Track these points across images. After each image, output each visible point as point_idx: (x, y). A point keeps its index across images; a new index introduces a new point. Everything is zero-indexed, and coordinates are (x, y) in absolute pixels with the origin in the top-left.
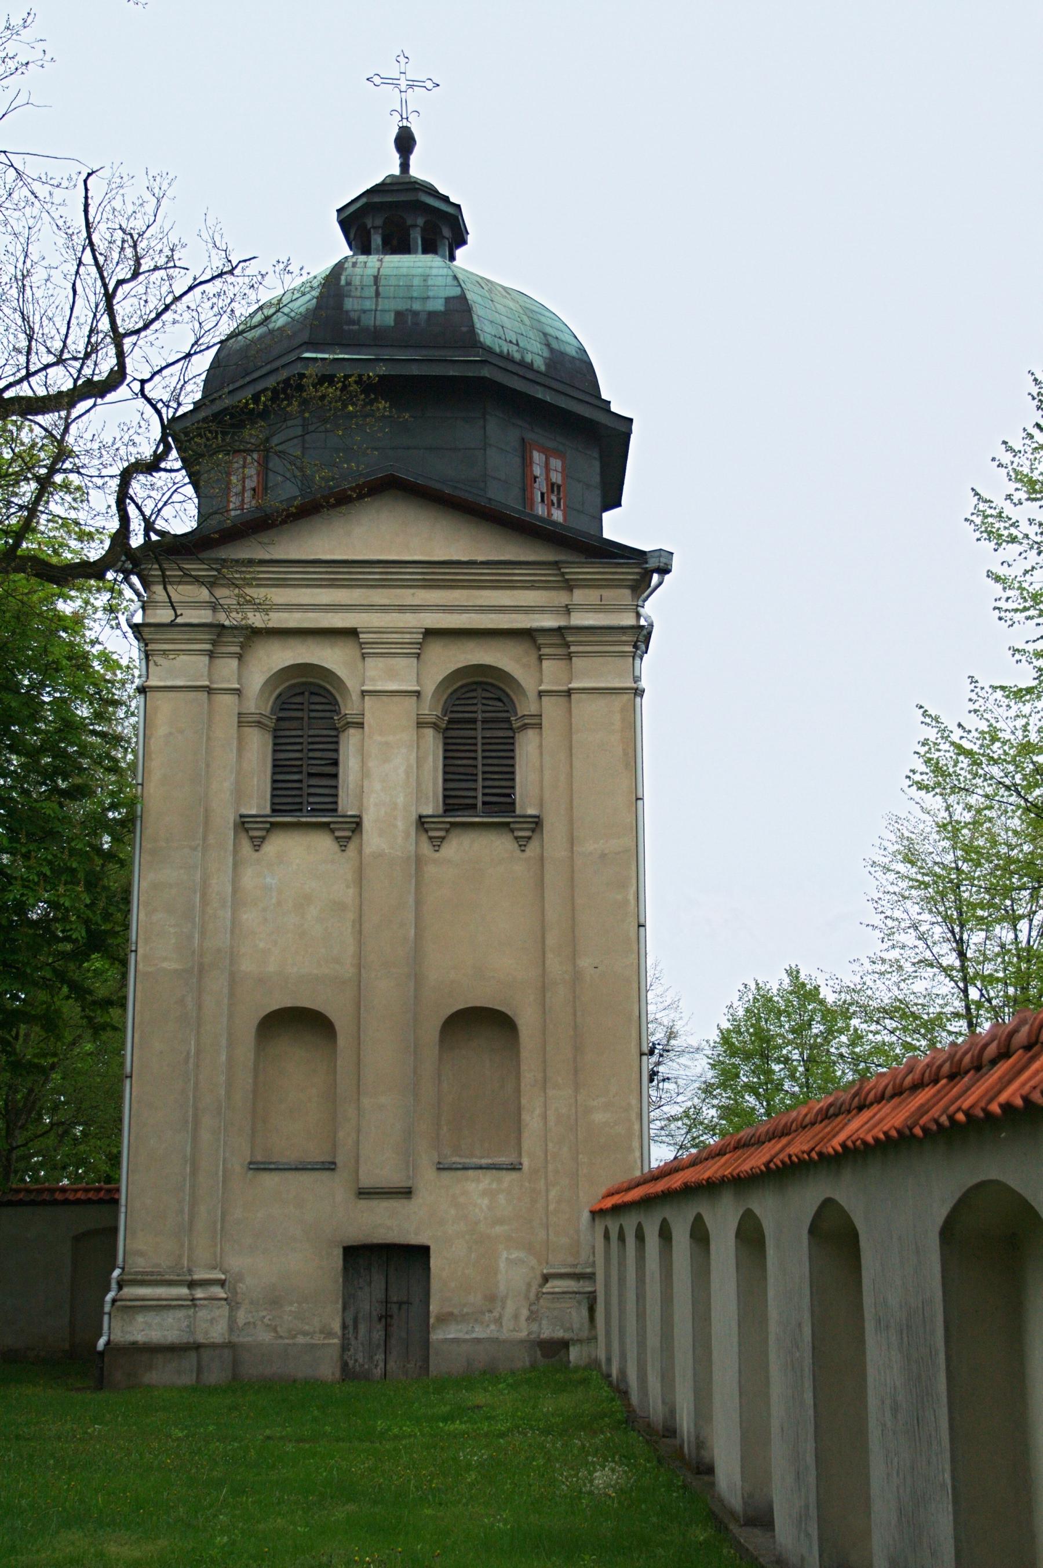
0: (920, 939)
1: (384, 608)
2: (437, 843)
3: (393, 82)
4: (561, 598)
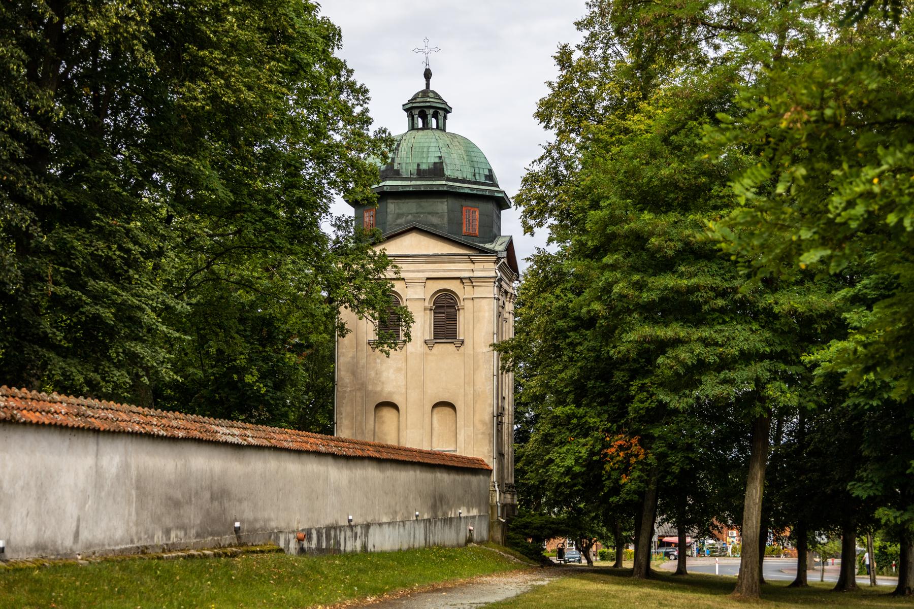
0: (819, 188)
1: (413, 271)
2: (431, 348)
3: (423, 50)
4: (471, 266)
